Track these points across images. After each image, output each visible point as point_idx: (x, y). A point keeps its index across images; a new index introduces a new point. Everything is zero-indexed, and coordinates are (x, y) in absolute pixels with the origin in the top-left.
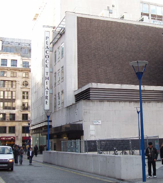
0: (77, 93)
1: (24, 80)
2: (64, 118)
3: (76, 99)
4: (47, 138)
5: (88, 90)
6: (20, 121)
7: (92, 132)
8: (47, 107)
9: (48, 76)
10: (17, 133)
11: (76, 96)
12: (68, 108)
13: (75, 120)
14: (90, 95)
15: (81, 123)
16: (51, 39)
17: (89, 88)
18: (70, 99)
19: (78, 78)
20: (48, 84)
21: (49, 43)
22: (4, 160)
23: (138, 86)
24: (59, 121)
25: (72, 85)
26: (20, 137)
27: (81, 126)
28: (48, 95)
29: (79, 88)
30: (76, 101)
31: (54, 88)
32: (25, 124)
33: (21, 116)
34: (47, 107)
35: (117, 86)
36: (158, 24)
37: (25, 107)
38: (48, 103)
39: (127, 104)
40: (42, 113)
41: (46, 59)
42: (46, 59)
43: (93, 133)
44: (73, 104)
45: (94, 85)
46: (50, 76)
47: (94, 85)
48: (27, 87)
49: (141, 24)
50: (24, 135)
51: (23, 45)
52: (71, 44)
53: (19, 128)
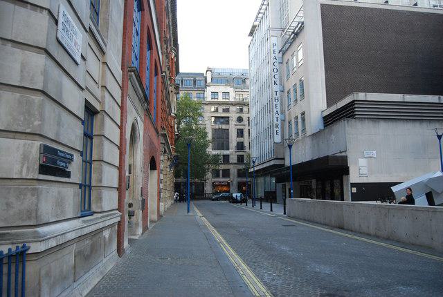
0: (326, 114)
1: (238, 115)
2: (307, 151)
3: (324, 124)
4: (276, 182)
5: (353, 103)
6: (235, 164)
7: (361, 171)
8: (278, 139)
9: (278, 96)
10: (232, 177)
11: (324, 118)
12: (315, 136)
13: (330, 149)
14: (353, 112)
15: (343, 154)
16: (277, 48)
17: (354, 101)
18: (315, 121)
19: (327, 94)
20: (279, 107)
21: (277, 52)
22: (10, 136)
23: (437, 97)
24: (301, 154)
25: (317, 104)
26: (235, 183)
27: (345, 159)
28: (279, 122)
29: (329, 105)
30: (325, 127)
31: (287, 112)
32: (241, 167)
33: (236, 158)
34: (278, 139)
35: (397, 97)
36: (441, 12)
37: (240, 146)
38: (279, 133)
39: (417, 124)
40: (268, 146)
41: (274, 74)
42: (274, 74)
43: (364, 171)
44: (320, 131)
45: (361, 96)
46: (281, 96)
47: (361, 96)
48: (242, 123)
49: (415, 10)
50: (240, 180)
51: (235, 75)
52: (314, 40)
53: (233, 170)
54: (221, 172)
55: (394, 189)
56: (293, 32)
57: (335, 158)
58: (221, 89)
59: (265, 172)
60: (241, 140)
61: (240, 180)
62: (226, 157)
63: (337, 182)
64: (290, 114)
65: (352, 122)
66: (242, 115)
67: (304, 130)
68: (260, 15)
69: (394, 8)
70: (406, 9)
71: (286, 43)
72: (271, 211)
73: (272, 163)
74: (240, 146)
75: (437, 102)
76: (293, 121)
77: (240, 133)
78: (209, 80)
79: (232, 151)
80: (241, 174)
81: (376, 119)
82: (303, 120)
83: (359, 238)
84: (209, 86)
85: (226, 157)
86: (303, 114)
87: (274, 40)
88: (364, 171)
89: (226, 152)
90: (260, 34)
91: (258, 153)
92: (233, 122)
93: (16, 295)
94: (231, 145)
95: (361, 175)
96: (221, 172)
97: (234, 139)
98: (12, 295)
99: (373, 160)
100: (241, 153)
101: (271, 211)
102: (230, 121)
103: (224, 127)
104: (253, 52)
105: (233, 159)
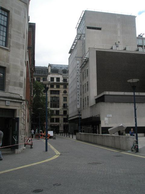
1: (64, 90)
5: (104, 96)
6: (62, 115)
10: (60, 122)
12: (92, 107)
13: (95, 114)
16: (79, 66)
18: (92, 101)
20: (79, 92)
21: (79, 67)
24: (86, 114)
26: (62, 125)
28: (79, 99)
29: (98, 94)
30: (96, 103)
32: (65, 117)
37: (65, 106)
38: (79, 104)
43: (107, 122)
44: (94, 105)
45: (107, 93)
47: (107, 93)
49: (137, 53)
50: (65, 123)
53: (61, 119)
54: (55, 120)
55: (109, 130)
56: (85, 61)
57: (95, 118)
58: (55, 76)
59: (73, 121)
60: (65, 102)
61: (65, 123)
62: (58, 112)
63: (97, 126)
64: (83, 96)
65: (102, 103)
66: (66, 90)
67: (88, 104)
68: (75, 44)
69: (128, 52)
70: (133, 52)
71: (82, 65)
72: (73, 138)
73: (77, 117)
74: (65, 106)
75: (138, 95)
76: (87, 98)
77: (65, 99)
78: (49, 71)
79: (61, 109)
80: (65, 120)
81: (112, 102)
82: (88, 99)
83: (98, 146)
84: (49, 74)
85: (58, 112)
86: (88, 97)
87: (78, 62)
88: (107, 122)
89: (58, 109)
90: (75, 53)
91: (72, 113)
92: (61, 94)
93: (144, 100)
94: (60, 105)
95: (105, 124)
96: (55, 120)
97: (62, 102)
98: (144, 100)
99: (110, 118)
100: (65, 110)
101: (73, 138)
102: (60, 93)
103: (57, 96)
104: (71, 61)
105: (61, 113)
